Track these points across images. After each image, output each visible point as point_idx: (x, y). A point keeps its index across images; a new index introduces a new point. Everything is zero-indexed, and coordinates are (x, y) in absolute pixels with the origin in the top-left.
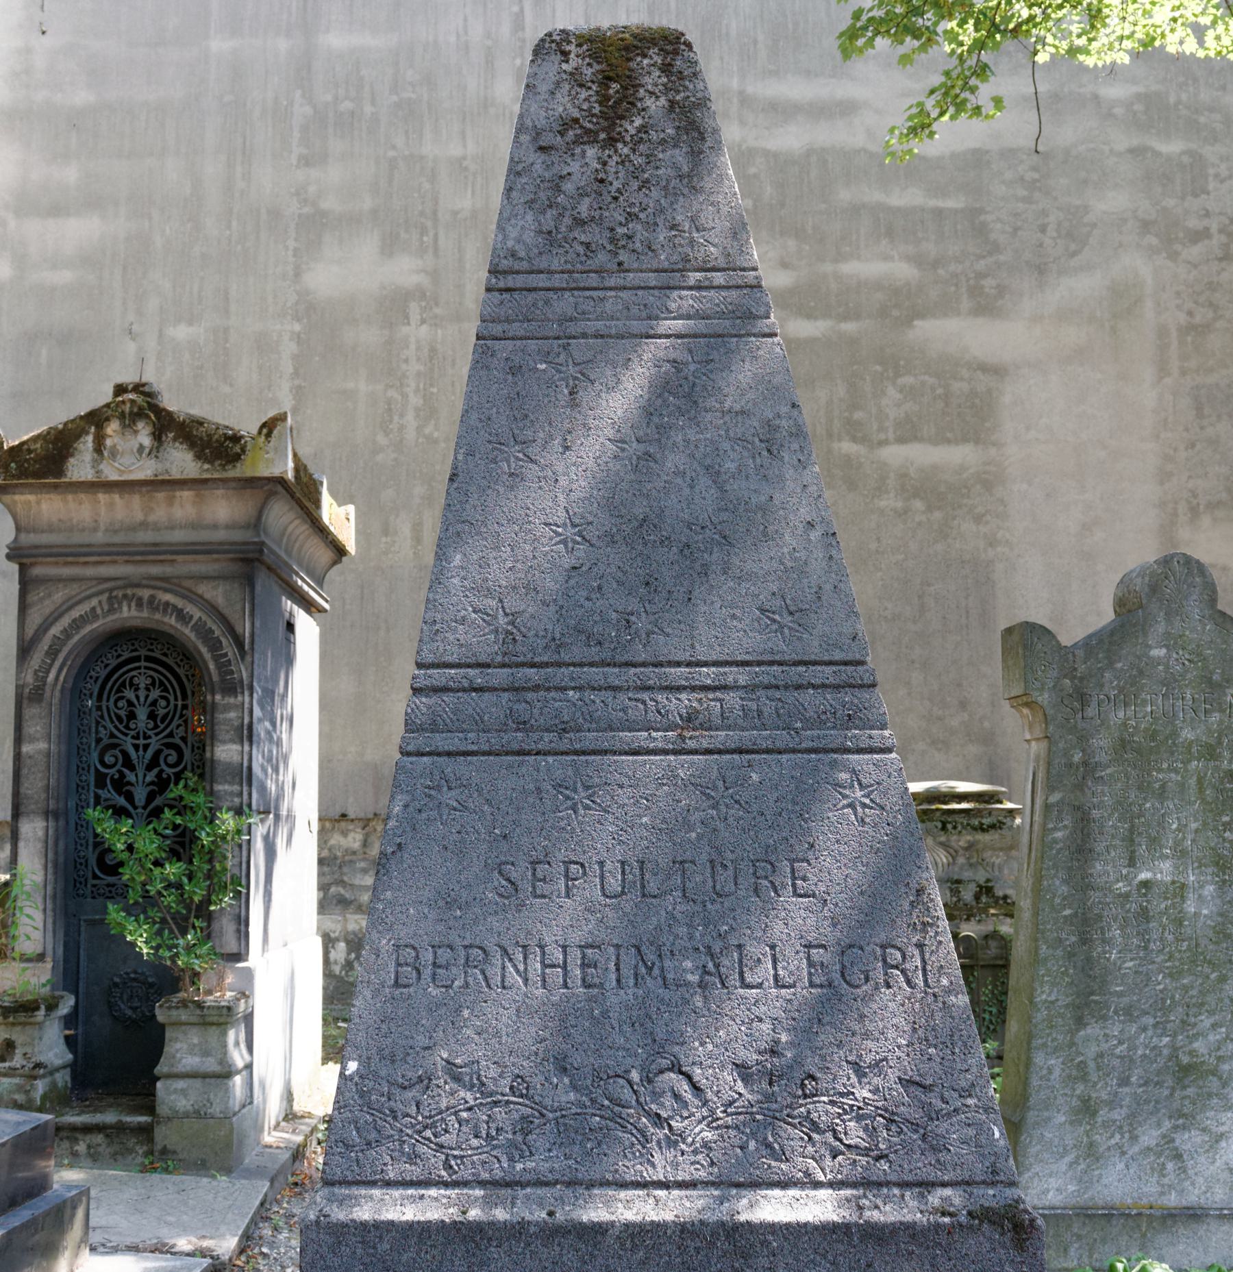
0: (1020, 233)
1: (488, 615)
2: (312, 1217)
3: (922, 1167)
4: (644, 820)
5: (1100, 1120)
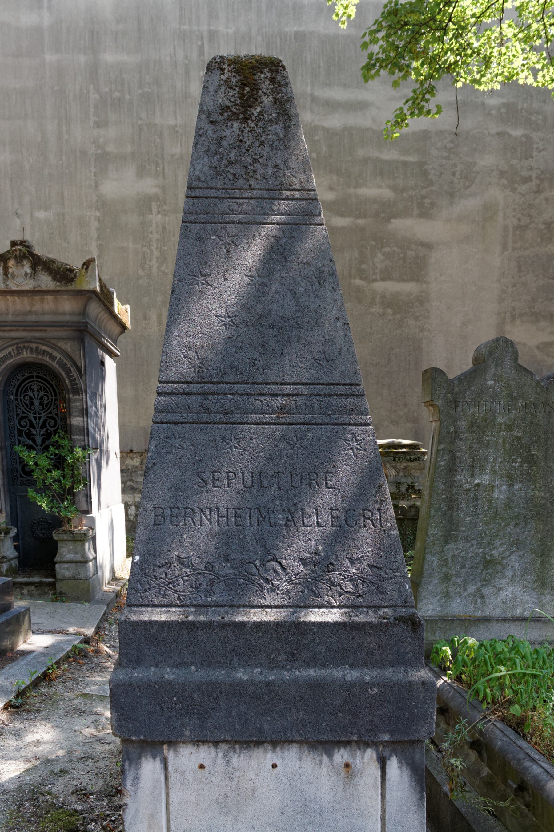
0: (443, 175)
1: (191, 359)
2: (123, 619)
3: (376, 600)
4: (262, 454)
5: (451, 582)
